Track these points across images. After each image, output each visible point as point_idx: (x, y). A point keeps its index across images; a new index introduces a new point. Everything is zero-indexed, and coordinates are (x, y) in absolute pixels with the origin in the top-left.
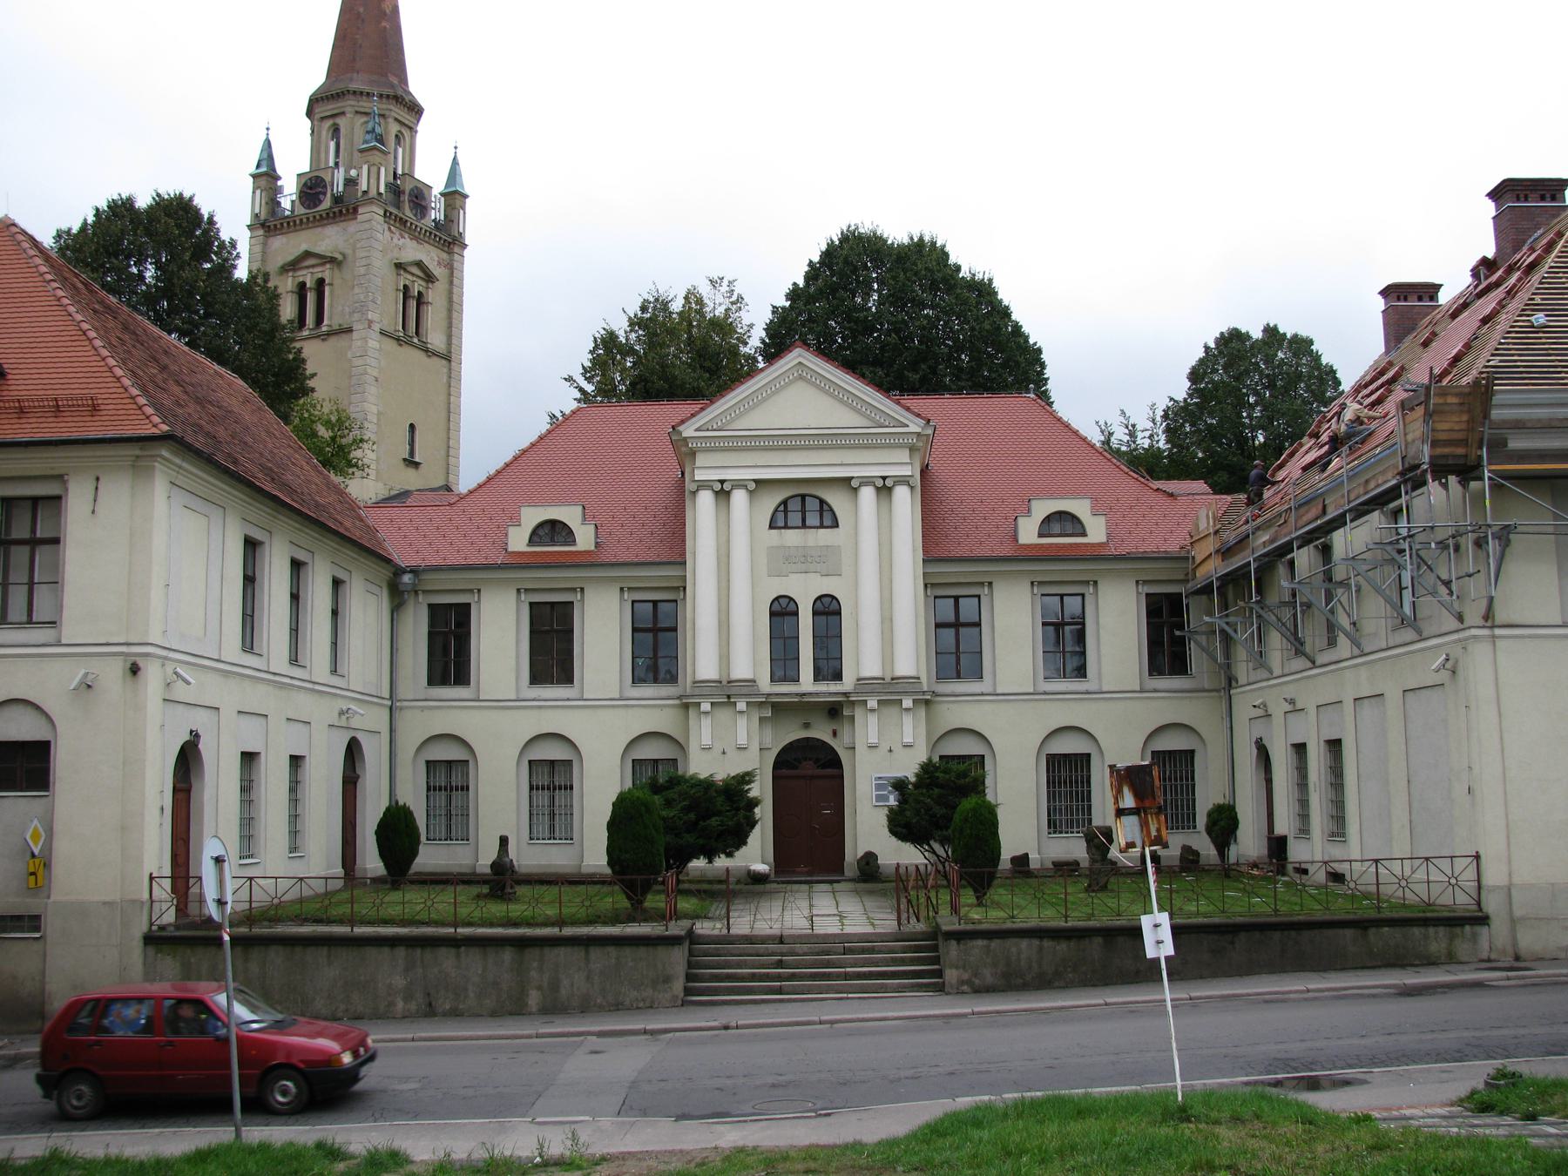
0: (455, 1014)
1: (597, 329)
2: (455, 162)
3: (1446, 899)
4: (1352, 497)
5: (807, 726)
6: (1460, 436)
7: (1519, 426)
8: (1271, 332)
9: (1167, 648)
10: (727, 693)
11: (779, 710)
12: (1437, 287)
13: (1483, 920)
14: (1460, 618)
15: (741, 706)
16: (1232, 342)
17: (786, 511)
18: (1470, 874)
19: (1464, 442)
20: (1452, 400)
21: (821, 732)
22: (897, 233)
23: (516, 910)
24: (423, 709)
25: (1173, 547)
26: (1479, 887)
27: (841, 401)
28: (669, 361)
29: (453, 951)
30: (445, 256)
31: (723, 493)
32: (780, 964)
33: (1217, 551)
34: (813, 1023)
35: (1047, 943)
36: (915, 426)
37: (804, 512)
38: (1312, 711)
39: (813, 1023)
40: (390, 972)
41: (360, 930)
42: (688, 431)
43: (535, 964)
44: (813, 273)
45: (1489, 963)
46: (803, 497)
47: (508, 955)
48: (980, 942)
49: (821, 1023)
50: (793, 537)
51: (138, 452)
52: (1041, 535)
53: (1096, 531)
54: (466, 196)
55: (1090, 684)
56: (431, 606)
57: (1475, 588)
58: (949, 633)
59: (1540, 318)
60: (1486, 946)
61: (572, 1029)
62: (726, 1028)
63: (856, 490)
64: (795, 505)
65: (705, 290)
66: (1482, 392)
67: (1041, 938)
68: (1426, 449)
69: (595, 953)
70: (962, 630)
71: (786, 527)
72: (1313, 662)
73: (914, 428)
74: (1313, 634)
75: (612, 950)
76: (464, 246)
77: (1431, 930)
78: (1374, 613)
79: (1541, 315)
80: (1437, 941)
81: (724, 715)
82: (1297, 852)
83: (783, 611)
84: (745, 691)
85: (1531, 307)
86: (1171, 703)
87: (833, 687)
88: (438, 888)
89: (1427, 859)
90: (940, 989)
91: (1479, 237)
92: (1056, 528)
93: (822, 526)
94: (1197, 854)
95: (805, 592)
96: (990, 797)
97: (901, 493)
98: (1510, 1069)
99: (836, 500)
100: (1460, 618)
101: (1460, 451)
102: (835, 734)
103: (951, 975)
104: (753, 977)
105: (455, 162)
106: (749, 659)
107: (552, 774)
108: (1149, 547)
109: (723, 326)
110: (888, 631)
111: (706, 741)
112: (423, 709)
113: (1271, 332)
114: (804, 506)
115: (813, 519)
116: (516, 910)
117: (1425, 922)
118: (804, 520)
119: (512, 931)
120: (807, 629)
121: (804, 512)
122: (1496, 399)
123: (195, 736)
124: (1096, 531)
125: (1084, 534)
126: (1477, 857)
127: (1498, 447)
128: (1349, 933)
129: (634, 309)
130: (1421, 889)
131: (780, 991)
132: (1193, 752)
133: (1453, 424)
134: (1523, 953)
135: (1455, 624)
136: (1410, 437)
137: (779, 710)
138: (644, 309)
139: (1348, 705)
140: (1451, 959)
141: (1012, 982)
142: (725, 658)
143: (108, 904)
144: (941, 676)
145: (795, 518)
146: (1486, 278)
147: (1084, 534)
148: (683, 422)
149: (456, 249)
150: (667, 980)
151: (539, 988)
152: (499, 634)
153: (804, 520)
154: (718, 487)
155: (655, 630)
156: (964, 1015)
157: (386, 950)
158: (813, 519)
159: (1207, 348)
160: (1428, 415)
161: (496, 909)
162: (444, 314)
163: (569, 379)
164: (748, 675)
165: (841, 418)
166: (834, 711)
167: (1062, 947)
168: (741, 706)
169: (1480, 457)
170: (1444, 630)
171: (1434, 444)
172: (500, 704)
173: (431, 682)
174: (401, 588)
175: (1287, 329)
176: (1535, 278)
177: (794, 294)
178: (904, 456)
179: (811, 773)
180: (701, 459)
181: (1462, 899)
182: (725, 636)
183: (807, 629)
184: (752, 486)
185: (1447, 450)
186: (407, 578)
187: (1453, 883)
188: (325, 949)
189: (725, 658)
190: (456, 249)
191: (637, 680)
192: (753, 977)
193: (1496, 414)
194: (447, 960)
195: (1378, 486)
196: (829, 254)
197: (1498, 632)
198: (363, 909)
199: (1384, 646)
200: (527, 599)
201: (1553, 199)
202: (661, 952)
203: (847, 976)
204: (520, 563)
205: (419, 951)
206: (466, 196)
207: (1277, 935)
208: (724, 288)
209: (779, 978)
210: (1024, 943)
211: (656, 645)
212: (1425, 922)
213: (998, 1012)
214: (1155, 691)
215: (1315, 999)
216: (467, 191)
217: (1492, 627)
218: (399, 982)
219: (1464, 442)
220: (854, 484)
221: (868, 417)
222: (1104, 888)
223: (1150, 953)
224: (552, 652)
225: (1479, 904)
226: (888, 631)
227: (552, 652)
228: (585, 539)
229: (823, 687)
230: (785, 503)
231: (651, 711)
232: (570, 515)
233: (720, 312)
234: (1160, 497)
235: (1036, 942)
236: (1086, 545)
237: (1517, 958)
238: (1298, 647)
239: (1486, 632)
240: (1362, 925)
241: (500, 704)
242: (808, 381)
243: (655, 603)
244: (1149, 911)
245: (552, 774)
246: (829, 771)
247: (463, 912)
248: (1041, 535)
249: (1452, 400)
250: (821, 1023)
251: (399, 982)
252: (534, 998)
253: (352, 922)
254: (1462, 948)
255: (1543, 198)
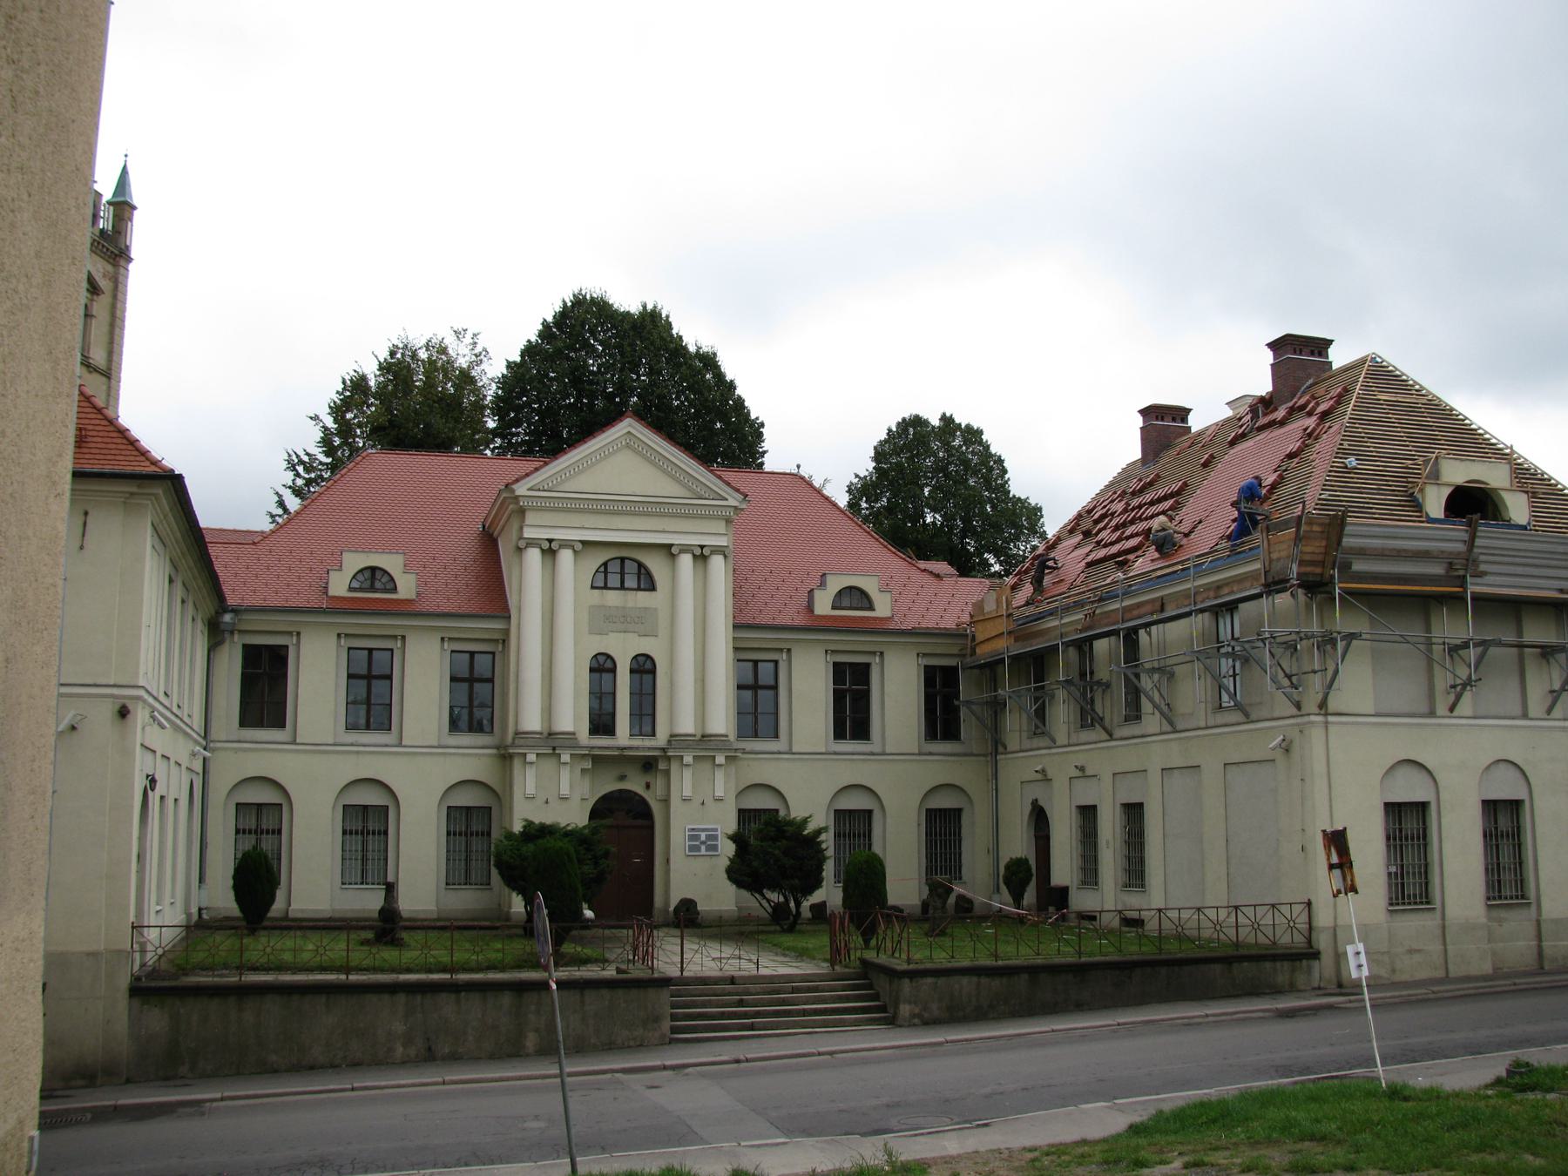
0: (454, 1058)
1: (347, 371)
2: (124, 172)
3: (1285, 939)
4: (1199, 598)
5: (622, 778)
6: (1320, 558)
7: (1362, 553)
8: (947, 420)
9: (941, 717)
10: (552, 742)
11: (599, 761)
12: (1188, 411)
13: (1316, 955)
14: (1298, 706)
15: (566, 757)
16: (913, 426)
17: (606, 572)
18: (1304, 917)
19: (1322, 563)
20: (1316, 528)
21: (635, 785)
22: (627, 300)
23: (408, 956)
24: (236, 750)
25: (949, 623)
26: (1311, 928)
27: (664, 471)
28: (405, 409)
29: (453, 996)
30: (110, 268)
31: (550, 551)
32: (741, 1003)
33: (1010, 633)
34: (812, 1055)
35: (984, 980)
36: (733, 500)
37: (622, 574)
38: (1107, 779)
39: (812, 1055)
40: (391, 1019)
41: (353, 978)
42: (521, 489)
43: (533, 1008)
44: (546, 332)
45: (1319, 990)
46: (623, 560)
47: (506, 999)
48: (930, 980)
49: (820, 1054)
50: (613, 598)
51: (134, 489)
52: (834, 608)
53: (883, 607)
54: (134, 208)
55: (874, 745)
56: (245, 646)
57: (1316, 683)
58: (748, 694)
59: (1352, 461)
60: (1317, 975)
61: (595, 1068)
62: (738, 1061)
63: (673, 556)
64: (614, 567)
65: (450, 341)
66: (1335, 525)
67: (979, 975)
68: (1295, 568)
69: (590, 995)
70: (760, 692)
71: (605, 587)
72: (1111, 735)
73: (732, 502)
74: (1111, 706)
75: (605, 992)
76: (130, 260)
77: (1278, 964)
78: (1192, 692)
79: (1352, 459)
80: (1282, 974)
81: (549, 765)
82: (1081, 901)
83: (602, 666)
84: (567, 743)
85: (1343, 453)
86: (945, 767)
87: (648, 742)
88: (277, 932)
89: (1273, 906)
90: (892, 1021)
91: (1257, 377)
92: (846, 602)
93: (639, 589)
94: (970, 901)
95: (623, 650)
96: (877, 848)
97: (717, 562)
98: (1525, 1059)
99: (655, 564)
100: (1298, 706)
101: (1318, 570)
102: (648, 786)
103: (905, 1010)
104: (722, 1016)
105: (124, 172)
106: (572, 716)
107: (365, 820)
108: (929, 622)
109: (466, 378)
110: (701, 695)
111: (531, 790)
112: (236, 750)
113: (947, 420)
114: (626, 569)
115: (631, 582)
116: (408, 956)
117: (1274, 958)
118: (622, 582)
119: (331, 977)
120: (625, 687)
121: (622, 574)
122: (1348, 529)
123: (1035, 803)
124: (883, 607)
125: (871, 608)
126: (1309, 904)
127: (1345, 567)
128: (1217, 968)
129: (384, 355)
130: (1232, 933)
131: (752, 1027)
132: (959, 811)
133: (1313, 548)
134: (1345, 982)
135: (1294, 711)
136: (1274, 556)
137: (599, 761)
138: (392, 354)
139: (1154, 777)
140: (1292, 989)
141: (956, 1014)
142: (548, 710)
143: (94, 955)
144: (741, 735)
145: (614, 580)
146: (1265, 415)
147: (871, 608)
148: (517, 481)
149: (122, 262)
150: (657, 1019)
151: (537, 1030)
152: (318, 676)
153: (622, 582)
154: (546, 545)
155: (369, 677)
156: (940, 1044)
157: (386, 997)
158: (631, 582)
159: (890, 430)
160: (1298, 539)
161: (389, 955)
162: (105, 329)
163: (316, 418)
164: (570, 728)
165: (663, 487)
166: (648, 765)
167: (996, 983)
168: (566, 757)
169: (1332, 577)
170: (1276, 714)
171: (1301, 563)
172: (317, 748)
173: (243, 723)
174: (222, 627)
175: (961, 419)
176: (1336, 427)
177: (529, 351)
178: (720, 527)
179: (626, 822)
180: (530, 518)
181: (1299, 939)
182: (548, 686)
183: (625, 687)
184: (579, 547)
185: (1309, 569)
186: (227, 618)
187: (1292, 926)
188: (323, 999)
189: (548, 710)
190: (122, 262)
191: (351, 727)
192: (722, 1016)
193: (1346, 541)
194: (447, 1006)
195: (1232, 592)
196: (563, 316)
197: (1330, 719)
198: (253, 956)
199: (1202, 724)
200: (832, 659)
201: (1320, 355)
202: (652, 993)
203: (805, 1013)
204: (339, 608)
205: (419, 997)
206: (134, 208)
207: (1164, 971)
208: (468, 339)
209: (745, 1015)
210: (965, 980)
211: (477, 698)
212: (1274, 958)
213: (1019, 1035)
214: (930, 754)
215: (1244, 1020)
216: (135, 202)
217: (1326, 714)
218: (399, 1027)
219: (1322, 563)
220: (674, 550)
221: (685, 486)
222: (943, 933)
223: (1354, 975)
224: (371, 698)
225: (1309, 941)
226: (701, 695)
227: (371, 698)
228: (406, 587)
229: (637, 742)
230: (605, 564)
231: (469, 760)
232: (391, 563)
233: (463, 362)
234: (927, 578)
235: (975, 979)
236: (875, 619)
237: (1340, 985)
238: (1088, 718)
239: (1320, 718)
240: (1228, 961)
241: (317, 748)
242: (635, 451)
243: (472, 654)
244: (1353, 942)
245: (365, 820)
246: (640, 822)
247: (459, 956)
248: (834, 608)
249: (1316, 528)
250: (820, 1054)
251: (399, 1027)
252: (531, 1041)
253: (347, 970)
254: (1301, 979)
255: (1312, 354)
